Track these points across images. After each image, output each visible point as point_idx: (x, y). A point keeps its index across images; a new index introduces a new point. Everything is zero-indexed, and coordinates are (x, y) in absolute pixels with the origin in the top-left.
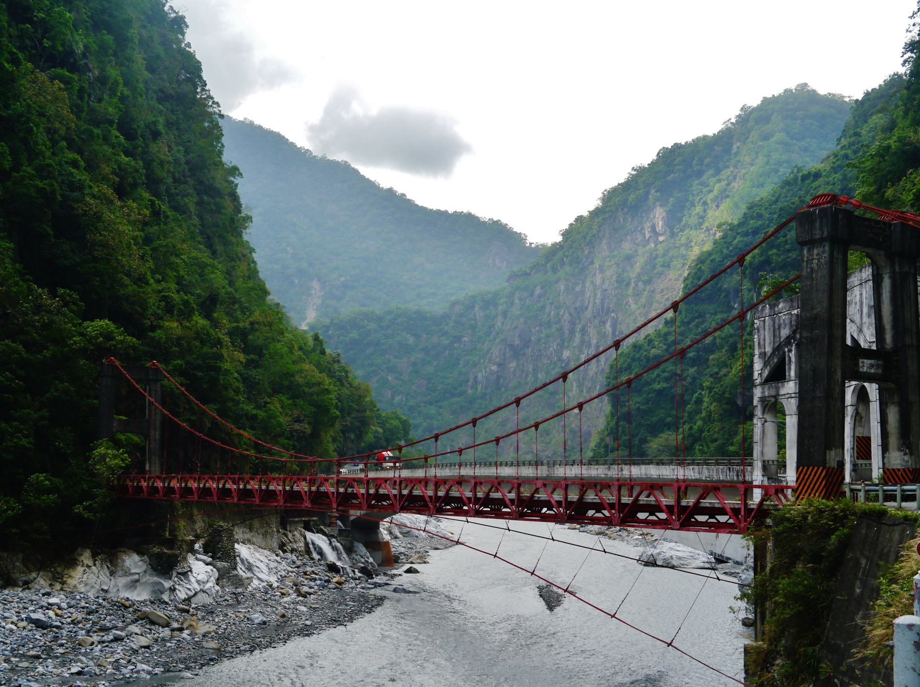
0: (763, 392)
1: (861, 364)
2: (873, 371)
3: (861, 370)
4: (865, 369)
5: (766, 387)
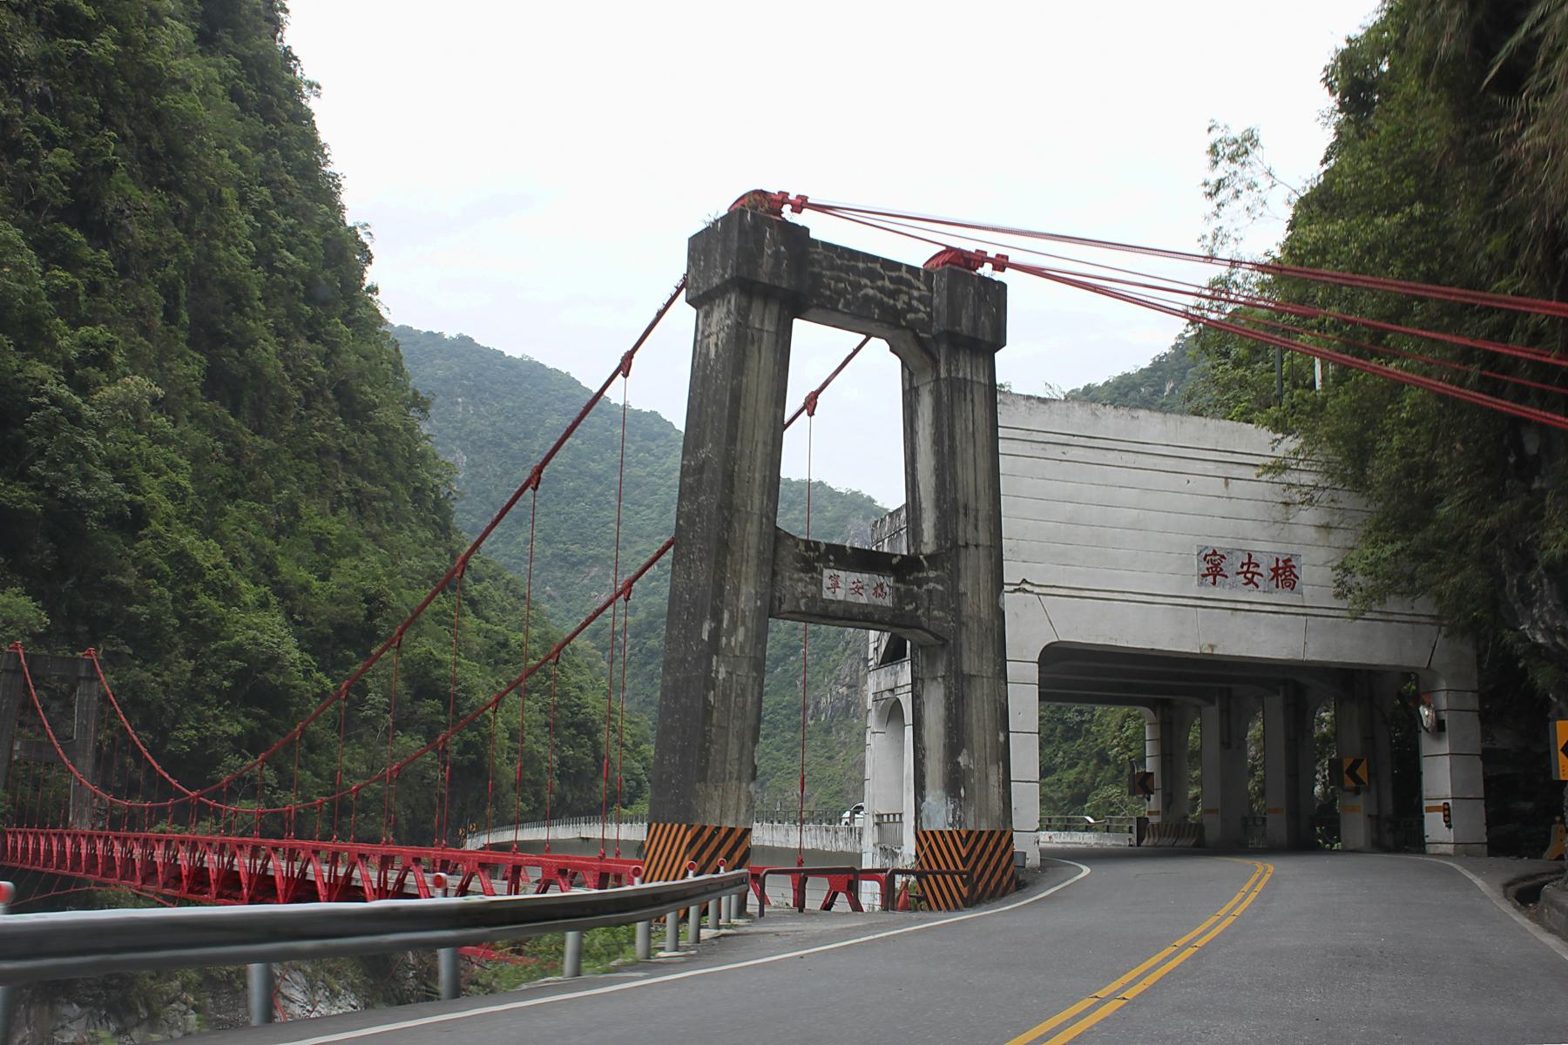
0: (878, 684)
1: (827, 582)
2: (863, 600)
3: (827, 595)
4: (840, 595)
5: (882, 671)
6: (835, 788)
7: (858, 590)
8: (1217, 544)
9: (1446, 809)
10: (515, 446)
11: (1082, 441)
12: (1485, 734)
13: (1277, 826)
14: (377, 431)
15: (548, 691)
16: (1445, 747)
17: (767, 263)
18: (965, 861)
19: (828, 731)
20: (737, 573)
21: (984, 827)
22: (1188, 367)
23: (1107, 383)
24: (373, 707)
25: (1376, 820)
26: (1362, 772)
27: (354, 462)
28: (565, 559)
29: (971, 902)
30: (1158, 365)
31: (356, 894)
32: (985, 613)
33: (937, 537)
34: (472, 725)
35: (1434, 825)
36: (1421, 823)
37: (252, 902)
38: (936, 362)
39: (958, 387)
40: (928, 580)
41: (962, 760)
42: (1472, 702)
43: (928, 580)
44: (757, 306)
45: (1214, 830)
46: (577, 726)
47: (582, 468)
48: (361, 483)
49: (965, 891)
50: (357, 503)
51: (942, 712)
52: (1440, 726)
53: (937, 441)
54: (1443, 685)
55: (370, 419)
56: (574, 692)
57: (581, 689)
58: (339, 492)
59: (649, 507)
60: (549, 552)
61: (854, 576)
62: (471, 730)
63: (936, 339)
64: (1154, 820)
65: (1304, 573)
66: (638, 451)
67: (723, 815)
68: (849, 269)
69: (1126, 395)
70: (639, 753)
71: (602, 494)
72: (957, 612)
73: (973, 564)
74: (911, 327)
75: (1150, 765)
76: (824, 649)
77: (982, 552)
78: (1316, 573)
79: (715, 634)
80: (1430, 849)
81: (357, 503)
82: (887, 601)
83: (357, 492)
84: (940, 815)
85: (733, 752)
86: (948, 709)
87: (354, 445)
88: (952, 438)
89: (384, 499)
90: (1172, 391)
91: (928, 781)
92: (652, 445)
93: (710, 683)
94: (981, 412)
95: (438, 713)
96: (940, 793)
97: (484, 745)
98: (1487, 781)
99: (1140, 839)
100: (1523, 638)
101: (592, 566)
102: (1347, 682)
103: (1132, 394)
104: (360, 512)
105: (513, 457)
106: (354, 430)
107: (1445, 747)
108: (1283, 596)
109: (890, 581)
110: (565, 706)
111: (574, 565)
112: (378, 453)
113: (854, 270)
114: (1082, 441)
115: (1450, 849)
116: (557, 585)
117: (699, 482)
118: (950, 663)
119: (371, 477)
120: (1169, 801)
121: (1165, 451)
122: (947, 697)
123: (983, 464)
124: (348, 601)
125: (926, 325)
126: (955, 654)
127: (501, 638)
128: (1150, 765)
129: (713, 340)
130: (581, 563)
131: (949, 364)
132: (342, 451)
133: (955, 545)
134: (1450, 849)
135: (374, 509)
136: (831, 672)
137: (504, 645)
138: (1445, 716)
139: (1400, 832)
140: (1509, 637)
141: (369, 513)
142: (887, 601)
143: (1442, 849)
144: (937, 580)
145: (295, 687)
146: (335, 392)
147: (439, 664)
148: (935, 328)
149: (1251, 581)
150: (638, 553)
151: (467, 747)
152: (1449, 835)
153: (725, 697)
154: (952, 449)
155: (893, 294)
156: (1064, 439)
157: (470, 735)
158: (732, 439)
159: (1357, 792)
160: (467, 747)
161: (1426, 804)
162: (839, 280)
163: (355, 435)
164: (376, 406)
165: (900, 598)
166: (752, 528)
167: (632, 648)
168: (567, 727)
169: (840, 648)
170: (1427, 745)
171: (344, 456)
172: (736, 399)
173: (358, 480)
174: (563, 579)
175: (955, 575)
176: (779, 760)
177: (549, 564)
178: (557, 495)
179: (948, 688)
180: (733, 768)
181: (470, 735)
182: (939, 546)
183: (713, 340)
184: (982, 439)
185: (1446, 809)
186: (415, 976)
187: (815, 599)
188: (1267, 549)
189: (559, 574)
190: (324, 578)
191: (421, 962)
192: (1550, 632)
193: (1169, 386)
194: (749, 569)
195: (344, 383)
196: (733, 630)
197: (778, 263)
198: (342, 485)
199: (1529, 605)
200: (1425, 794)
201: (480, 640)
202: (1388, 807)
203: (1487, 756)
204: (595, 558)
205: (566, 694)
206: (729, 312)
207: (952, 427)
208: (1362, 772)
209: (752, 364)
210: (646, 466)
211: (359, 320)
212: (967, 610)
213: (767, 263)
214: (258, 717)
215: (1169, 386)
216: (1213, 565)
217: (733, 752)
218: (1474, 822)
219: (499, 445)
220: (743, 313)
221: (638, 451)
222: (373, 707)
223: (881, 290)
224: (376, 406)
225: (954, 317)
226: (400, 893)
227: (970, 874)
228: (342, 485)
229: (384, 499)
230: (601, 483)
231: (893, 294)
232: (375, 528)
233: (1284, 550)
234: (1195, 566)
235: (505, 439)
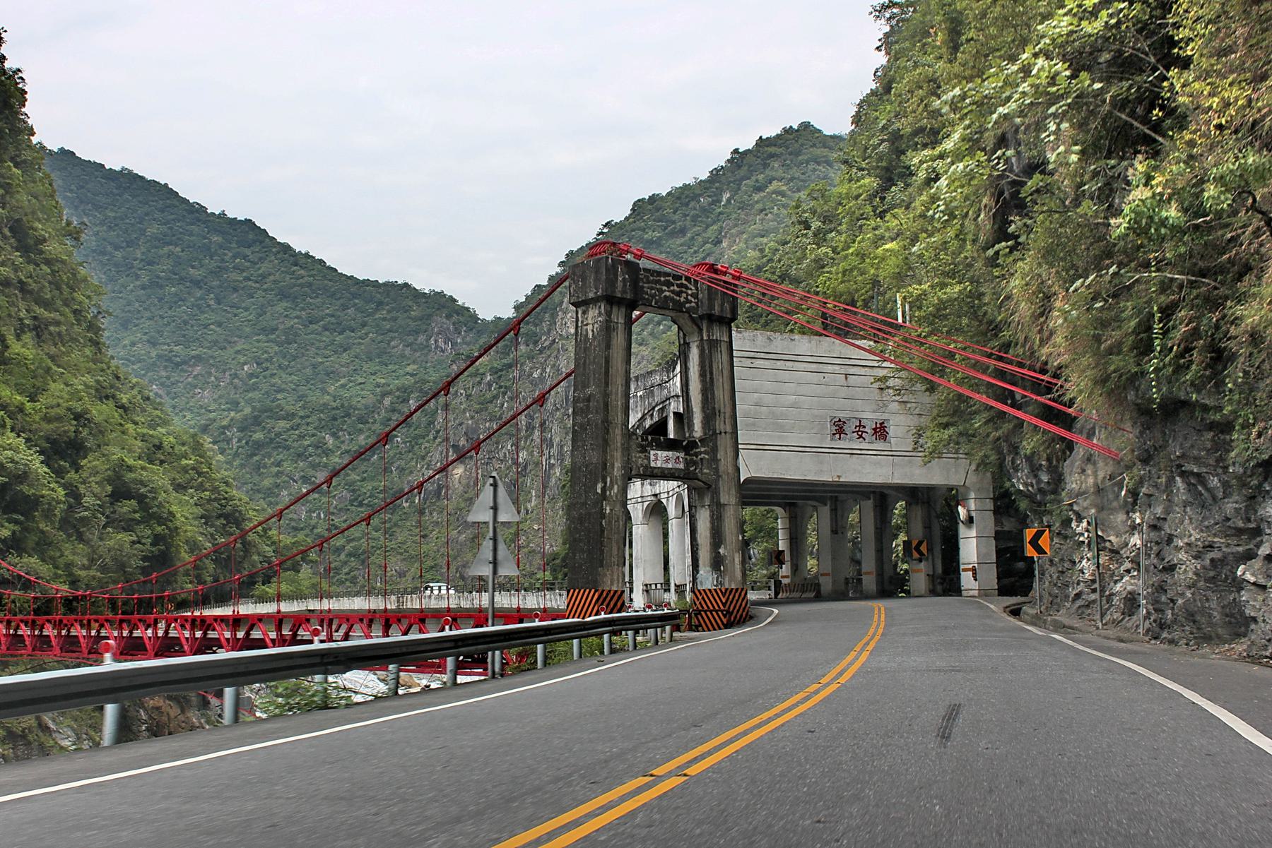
1: (652, 458)
3: (653, 464)
6: (429, 563)
7: (667, 461)
8: (841, 415)
9: (974, 569)
10: (119, 254)
11: (762, 355)
12: (997, 522)
13: (869, 582)
14: (48, 262)
15: (201, 487)
16: (973, 533)
17: (620, 285)
18: (724, 605)
19: (421, 512)
20: (612, 456)
21: (733, 586)
22: (743, 179)
23: (669, 194)
24: (87, 509)
25: (932, 577)
26: (923, 548)
27: (31, 292)
28: (169, 360)
29: (729, 625)
30: (716, 174)
31: (261, 644)
32: (730, 470)
33: (703, 428)
34: (161, 520)
35: (967, 580)
36: (959, 579)
37: (157, 655)
38: (701, 330)
39: (713, 344)
40: (701, 453)
41: (721, 551)
42: (990, 505)
43: (701, 453)
44: (615, 309)
45: (827, 585)
46: (226, 516)
47: (183, 274)
48: (40, 311)
49: (725, 621)
50: (36, 328)
51: (708, 524)
52: (970, 520)
53: (702, 374)
54: (973, 495)
55: (41, 252)
56: (223, 487)
57: (227, 483)
58: (21, 320)
59: (246, 309)
60: (154, 354)
61: (665, 454)
62: (160, 525)
63: (701, 317)
64: (785, 581)
65: (892, 430)
66: (235, 257)
67: (612, 584)
68: (658, 282)
69: (687, 205)
70: (269, 538)
71: (200, 299)
72: (717, 470)
73: (724, 443)
74: (688, 311)
75: (782, 546)
76: (416, 438)
77: (728, 436)
78: (900, 427)
79: (604, 489)
80: (964, 593)
81: (36, 328)
82: (681, 466)
83: (35, 318)
84: (707, 579)
85: (615, 551)
86: (712, 522)
87: (31, 277)
88: (711, 373)
89: (58, 323)
90: (729, 201)
91: (701, 562)
92: (247, 251)
93: (603, 516)
94: (725, 357)
95: (135, 512)
96: (708, 568)
97: (172, 537)
98: (998, 552)
99: (776, 594)
100: (1013, 486)
101: (195, 365)
102: (916, 495)
103: (692, 204)
104: (38, 336)
105: (116, 265)
106: (28, 263)
107: (973, 533)
108: (880, 445)
109: (682, 455)
110: (215, 499)
111: (178, 364)
112: (50, 283)
113: (658, 282)
114: (762, 355)
115: (976, 593)
116: (162, 384)
117: (588, 406)
118: (712, 498)
119: (47, 305)
120: (795, 568)
121: (810, 359)
122: (712, 517)
123: (727, 387)
124: (59, 419)
125: (695, 310)
126: (716, 494)
127: (156, 442)
128: (782, 546)
129: (590, 327)
130: (184, 362)
131: (708, 331)
132: (20, 281)
133: (715, 433)
134: (976, 593)
135: (51, 334)
136: (423, 458)
137: (159, 447)
138: (973, 514)
139: (947, 581)
140: (1007, 484)
141: (46, 336)
142: (681, 466)
143: (971, 593)
144: (705, 452)
145: (43, 497)
146: (11, 229)
147: (130, 469)
148: (700, 312)
149: (861, 436)
150: (238, 352)
151: (157, 539)
152: (975, 585)
153: (610, 522)
154: (712, 379)
155: (679, 294)
156: (752, 355)
157: (159, 529)
158: (607, 384)
159: (920, 561)
160: (157, 539)
161: (962, 567)
162: (652, 289)
163: (31, 267)
164: (45, 240)
165: (687, 463)
166: (618, 432)
167: (239, 441)
168: (219, 517)
169: (431, 437)
170: (963, 531)
171: (22, 286)
172: (607, 362)
173: (36, 308)
174: (168, 378)
175: (714, 450)
176: (378, 539)
177: (154, 364)
178: (160, 300)
179: (712, 511)
180: (615, 559)
181: (159, 529)
182: (705, 434)
183: (590, 327)
184: (726, 373)
185: (974, 569)
186: (147, 729)
187: (647, 467)
188: (870, 417)
189: (164, 374)
190: (33, 399)
191: (151, 718)
192: (1026, 484)
193: (726, 196)
194: (618, 454)
195: (18, 221)
196: (612, 487)
197: (625, 285)
198: (23, 314)
199: (1016, 470)
200: (961, 561)
201: (139, 443)
202: (939, 570)
203: (998, 536)
204: (198, 358)
205: (215, 490)
206: (600, 313)
207: (711, 367)
208: (923, 548)
209: (614, 342)
210: (243, 271)
211: (25, 161)
212: (722, 468)
213: (620, 285)
214: (16, 522)
215: (726, 196)
216: (839, 429)
217: (615, 551)
218: (990, 577)
219: (103, 253)
220: (609, 314)
221: (235, 257)
222: (87, 509)
223: (673, 292)
224: (45, 240)
225: (711, 306)
226: (294, 641)
227: (728, 611)
228: (23, 314)
229: (58, 323)
230: (200, 288)
231: (679, 294)
232: (53, 350)
233: (880, 416)
234: (829, 428)
235: (109, 248)
